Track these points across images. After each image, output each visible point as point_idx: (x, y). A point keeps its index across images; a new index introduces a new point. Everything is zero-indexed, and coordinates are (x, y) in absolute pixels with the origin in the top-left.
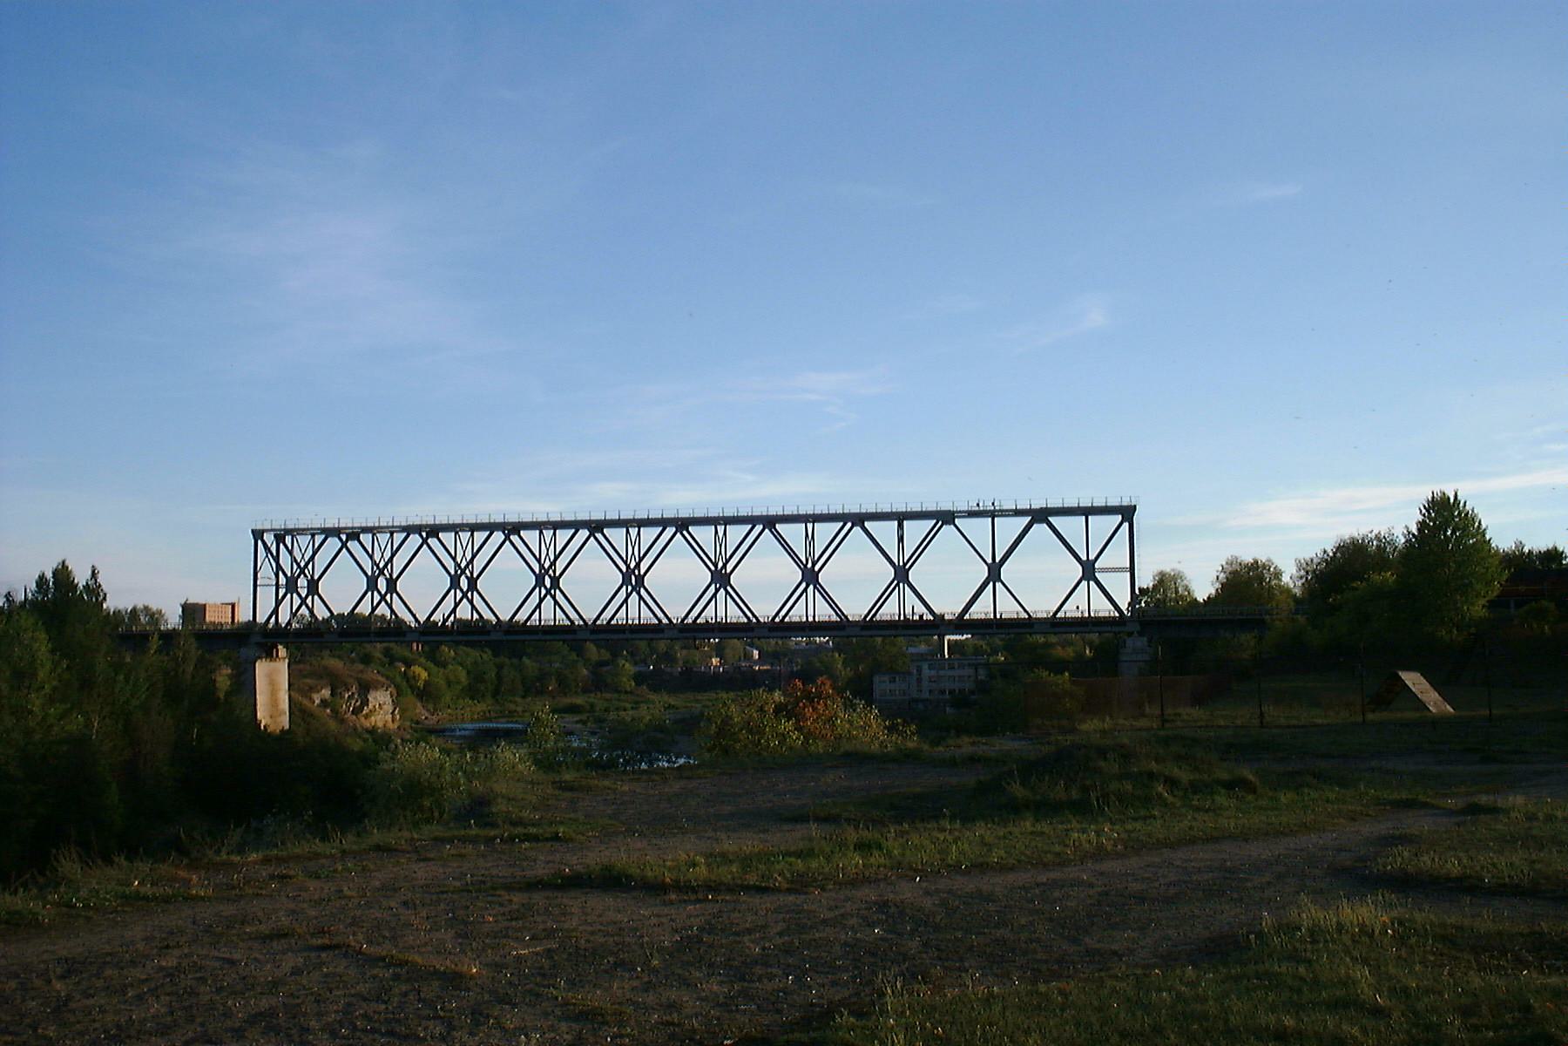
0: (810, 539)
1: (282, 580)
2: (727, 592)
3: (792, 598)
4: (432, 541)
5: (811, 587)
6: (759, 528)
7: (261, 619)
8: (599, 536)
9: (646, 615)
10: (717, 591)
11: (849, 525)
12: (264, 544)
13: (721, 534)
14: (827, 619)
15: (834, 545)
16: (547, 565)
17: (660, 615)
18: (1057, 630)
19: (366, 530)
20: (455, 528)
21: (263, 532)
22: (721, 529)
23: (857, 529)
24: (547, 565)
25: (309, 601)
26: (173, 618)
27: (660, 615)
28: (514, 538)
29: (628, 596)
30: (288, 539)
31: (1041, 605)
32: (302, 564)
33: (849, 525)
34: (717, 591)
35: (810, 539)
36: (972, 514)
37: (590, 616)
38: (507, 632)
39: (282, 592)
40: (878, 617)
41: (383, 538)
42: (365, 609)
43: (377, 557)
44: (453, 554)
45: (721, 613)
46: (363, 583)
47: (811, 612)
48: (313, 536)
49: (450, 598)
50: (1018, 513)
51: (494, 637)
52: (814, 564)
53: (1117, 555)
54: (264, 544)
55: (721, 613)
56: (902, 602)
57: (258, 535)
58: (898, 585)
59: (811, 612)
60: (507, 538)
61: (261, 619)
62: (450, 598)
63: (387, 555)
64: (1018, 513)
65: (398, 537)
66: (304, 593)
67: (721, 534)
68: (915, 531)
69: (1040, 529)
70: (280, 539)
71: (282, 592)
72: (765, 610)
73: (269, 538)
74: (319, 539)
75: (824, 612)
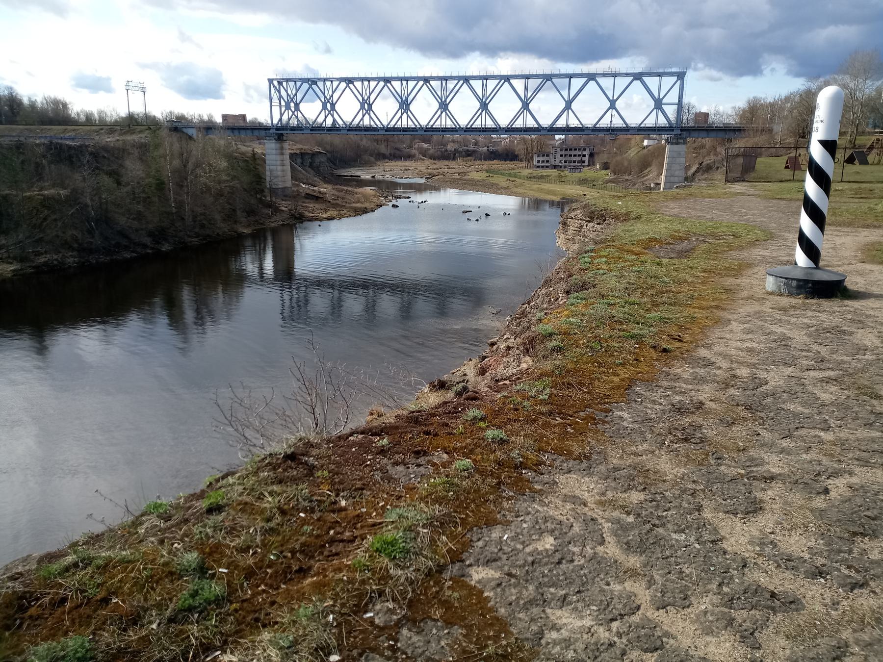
0: (484, 88)
1: (283, 103)
2: (408, 116)
3: (474, 117)
4: (314, 87)
5: (444, 114)
6: (461, 82)
7: (284, 122)
8: (389, 85)
9: (411, 125)
10: (442, 113)
11: (503, 81)
12: (274, 86)
13: (444, 84)
14: (532, 126)
15: (496, 90)
16: (366, 98)
17: (416, 123)
18: (640, 133)
19: (320, 79)
20: (362, 80)
21: (273, 80)
22: (444, 82)
23: (506, 83)
24: (366, 98)
25: (296, 113)
26: (219, 120)
27: (416, 123)
28: (351, 86)
29: (402, 114)
30: (284, 84)
31: (589, 121)
32: (292, 96)
33: (503, 81)
34: (442, 113)
35: (484, 88)
36: (605, 75)
37: (385, 123)
38: (386, 131)
39: (283, 109)
40: (514, 126)
41: (328, 83)
42: (320, 120)
43: (289, 92)
44: (323, 91)
45: (443, 123)
46: (337, 107)
47: (483, 123)
48: (295, 82)
49: (323, 115)
50: (627, 75)
51: (419, 133)
52: (487, 99)
53: (673, 97)
54: (274, 86)
55: (443, 123)
56: (525, 119)
57: (271, 81)
58: (523, 111)
59: (483, 123)
60: (348, 86)
61: (275, 121)
62: (323, 115)
63: (294, 92)
64: (627, 75)
65: (335, 84)
66: (293, 109)
67: (444, 84)
68: (491, 84)
69: (592, 83)
70: (280, 83)
71: (283, 109)
72: (463, 122)
73: (275, 83)
74: (299, 84)
75: (531, 123)
